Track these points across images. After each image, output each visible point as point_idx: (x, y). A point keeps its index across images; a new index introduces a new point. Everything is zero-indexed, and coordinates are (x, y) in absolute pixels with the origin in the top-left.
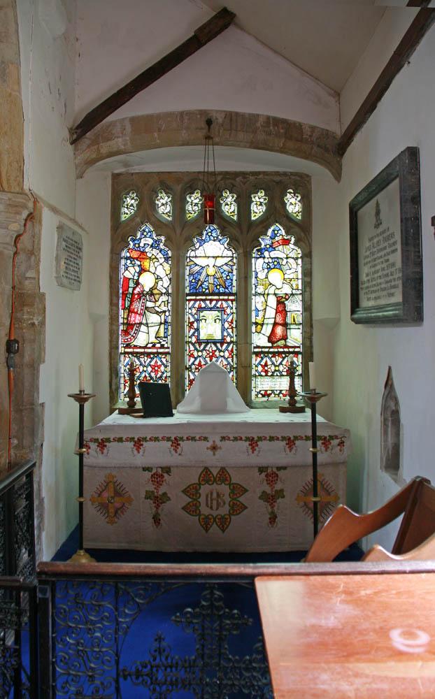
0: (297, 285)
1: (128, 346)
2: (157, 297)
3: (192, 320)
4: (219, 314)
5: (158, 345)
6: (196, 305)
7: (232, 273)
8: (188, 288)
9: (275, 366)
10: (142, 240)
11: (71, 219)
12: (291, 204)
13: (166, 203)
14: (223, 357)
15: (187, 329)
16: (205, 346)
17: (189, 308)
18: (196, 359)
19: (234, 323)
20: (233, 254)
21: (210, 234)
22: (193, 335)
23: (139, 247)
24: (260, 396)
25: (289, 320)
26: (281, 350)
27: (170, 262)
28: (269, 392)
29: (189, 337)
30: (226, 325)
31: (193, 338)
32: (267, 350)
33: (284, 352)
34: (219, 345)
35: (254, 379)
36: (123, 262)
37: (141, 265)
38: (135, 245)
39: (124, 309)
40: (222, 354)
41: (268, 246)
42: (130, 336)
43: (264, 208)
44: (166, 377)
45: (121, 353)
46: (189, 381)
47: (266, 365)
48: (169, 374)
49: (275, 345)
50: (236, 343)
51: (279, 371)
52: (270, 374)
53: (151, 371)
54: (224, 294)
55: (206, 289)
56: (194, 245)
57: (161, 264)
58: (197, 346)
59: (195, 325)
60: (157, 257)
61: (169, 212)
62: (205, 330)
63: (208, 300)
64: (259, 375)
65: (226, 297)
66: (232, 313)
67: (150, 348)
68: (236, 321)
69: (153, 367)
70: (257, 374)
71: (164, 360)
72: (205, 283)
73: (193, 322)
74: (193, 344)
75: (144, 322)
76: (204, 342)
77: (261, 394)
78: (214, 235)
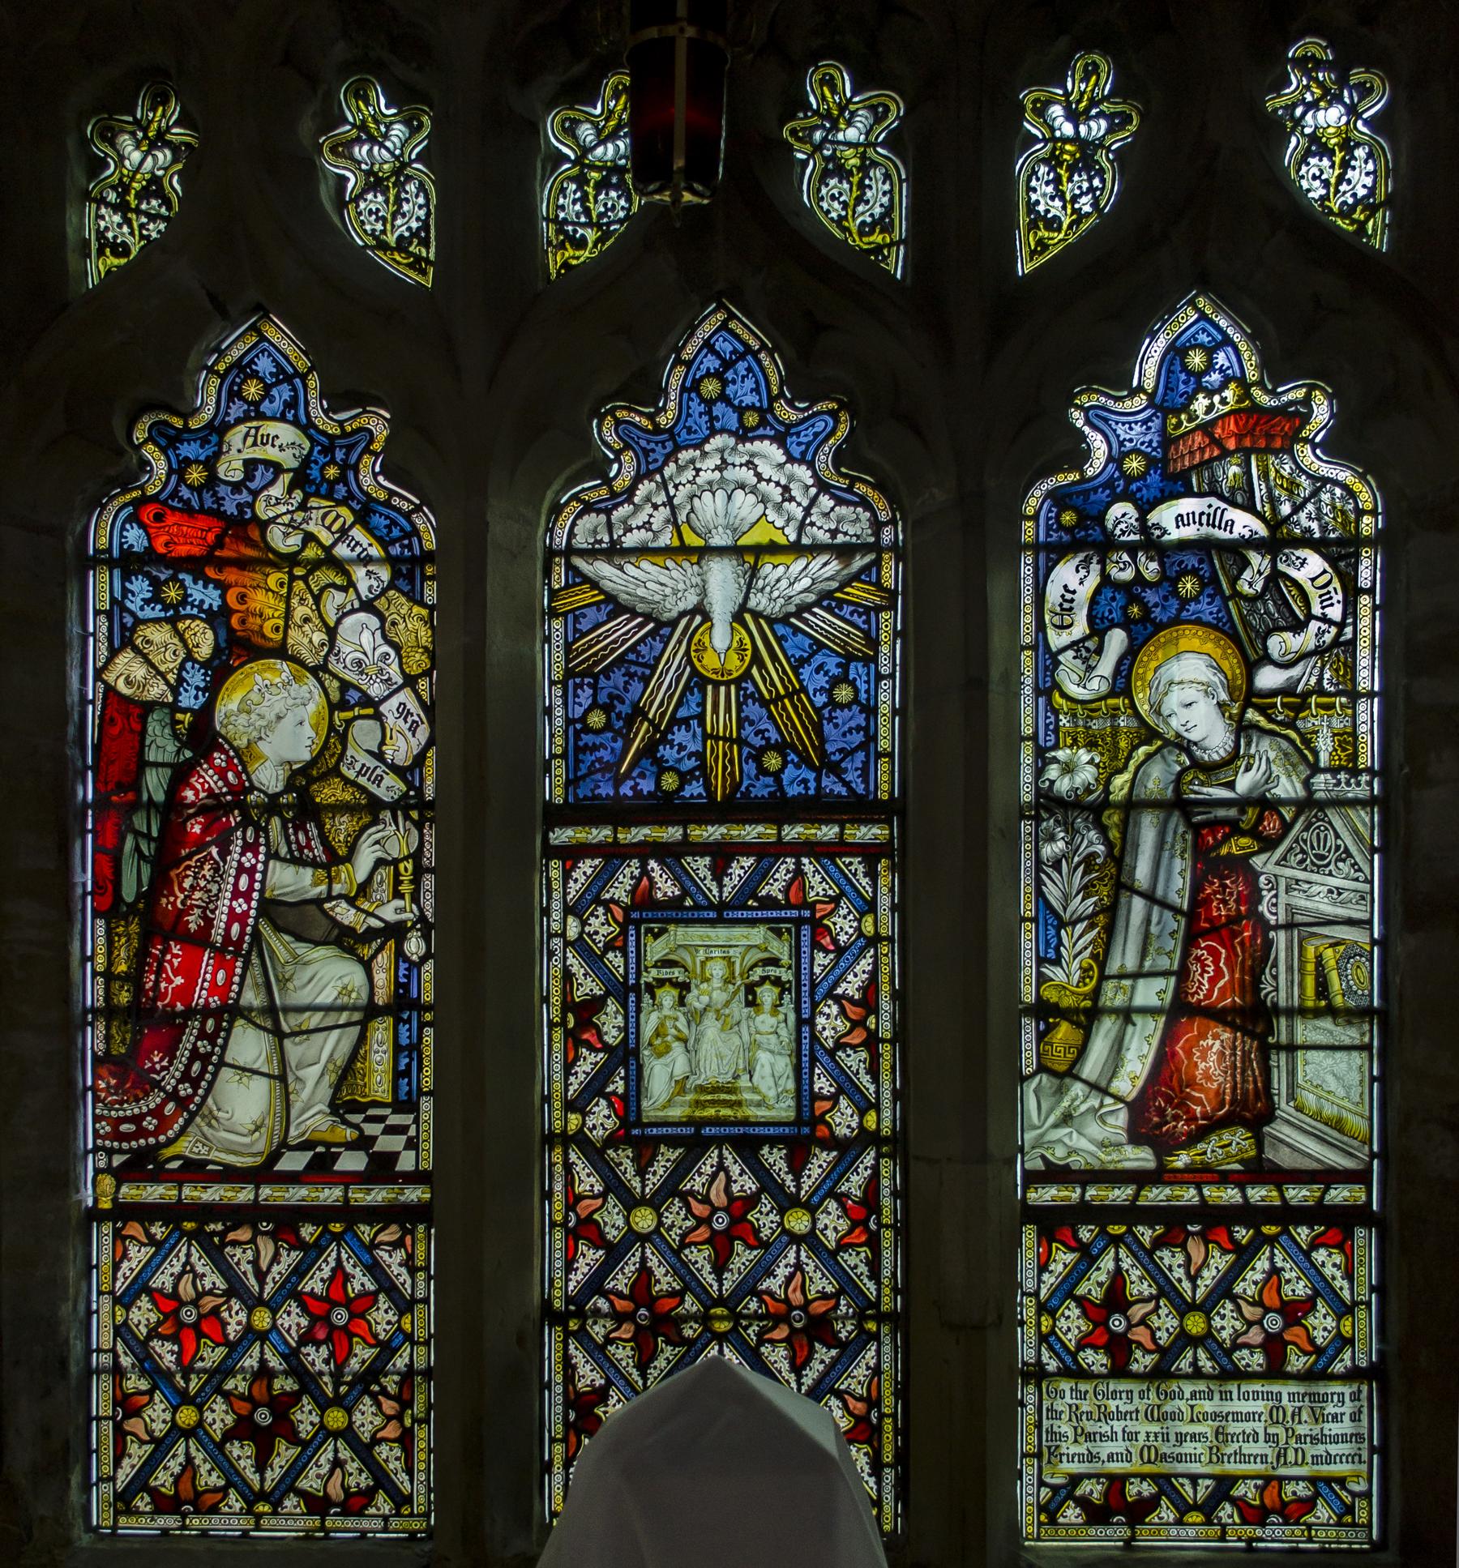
0: (1348, 739)
1: (144, 1165)
2: (342, 827)
3: (587, 986)
4: (781, 949)
5: (352, 1162)
6: (620, 890)
7: (871, 660)
8: (559, 769)
9: (1184, 1308)
10: (235, 436)
11: (1110, 930)
12: (1317, 145)
13: (401, 169)
14: (811, 1240)
15: (552, 1047)
16: (681, 1170)
17: (568, 910)
18: (615, 1253)
19: (885, 1005)
20: (877, 526)
21: (711, 388)
22: (596, 1087)
23: (212, 480)
24: (1071, 1514)
25: (1280, 987)
26: (1230, 1195)
27: (430, 593)
28: (1136, 1489)
29: (570, 1106)
30: (830, 1023)
31: (601, 1109)
32: (1120, 1195)
33: (1247, 1214)
34: (775, 1158)
35: (1029, 1395)
36: (100, 587)
37: (225, 611)
38: (179, 470)
39: (112, 910)
40: (798, 1222)
41: (1134, 465)
42: (154, 1100)
43: (1111, 186)
44: (409, 1374)
45: (95, 1215)
46: (568, 1404)
47: (1116, 1297)
48: (423, 1358)
49: (1181, 1160)
50: (896, 1145)
51: (1206, 1339)
52: (1143, 1361)
53: (306, 1338)
54: (815, 808)
55: (684, 778)
56: (598, 471)
57: (368, 606)
58: (624, 1160)
59: (611, 1023)
60: (342, 551)
61: (420, 235)
62: (678, 1062)
63: (701, 849)
64: (1065, 1372)
65: (828, 832)
66: (875, 940)
67: (292, 1178)
68: (895, 996)
69: (317, 1309)
70: (1052, 1365)
71: (393, 1261)
72: (680, 736)
73: (595, 1005)
74: (596, 1154)
75: (251, 997)
76: (673, 1142)
77: (1084, 1503)
78: (744, 392)
